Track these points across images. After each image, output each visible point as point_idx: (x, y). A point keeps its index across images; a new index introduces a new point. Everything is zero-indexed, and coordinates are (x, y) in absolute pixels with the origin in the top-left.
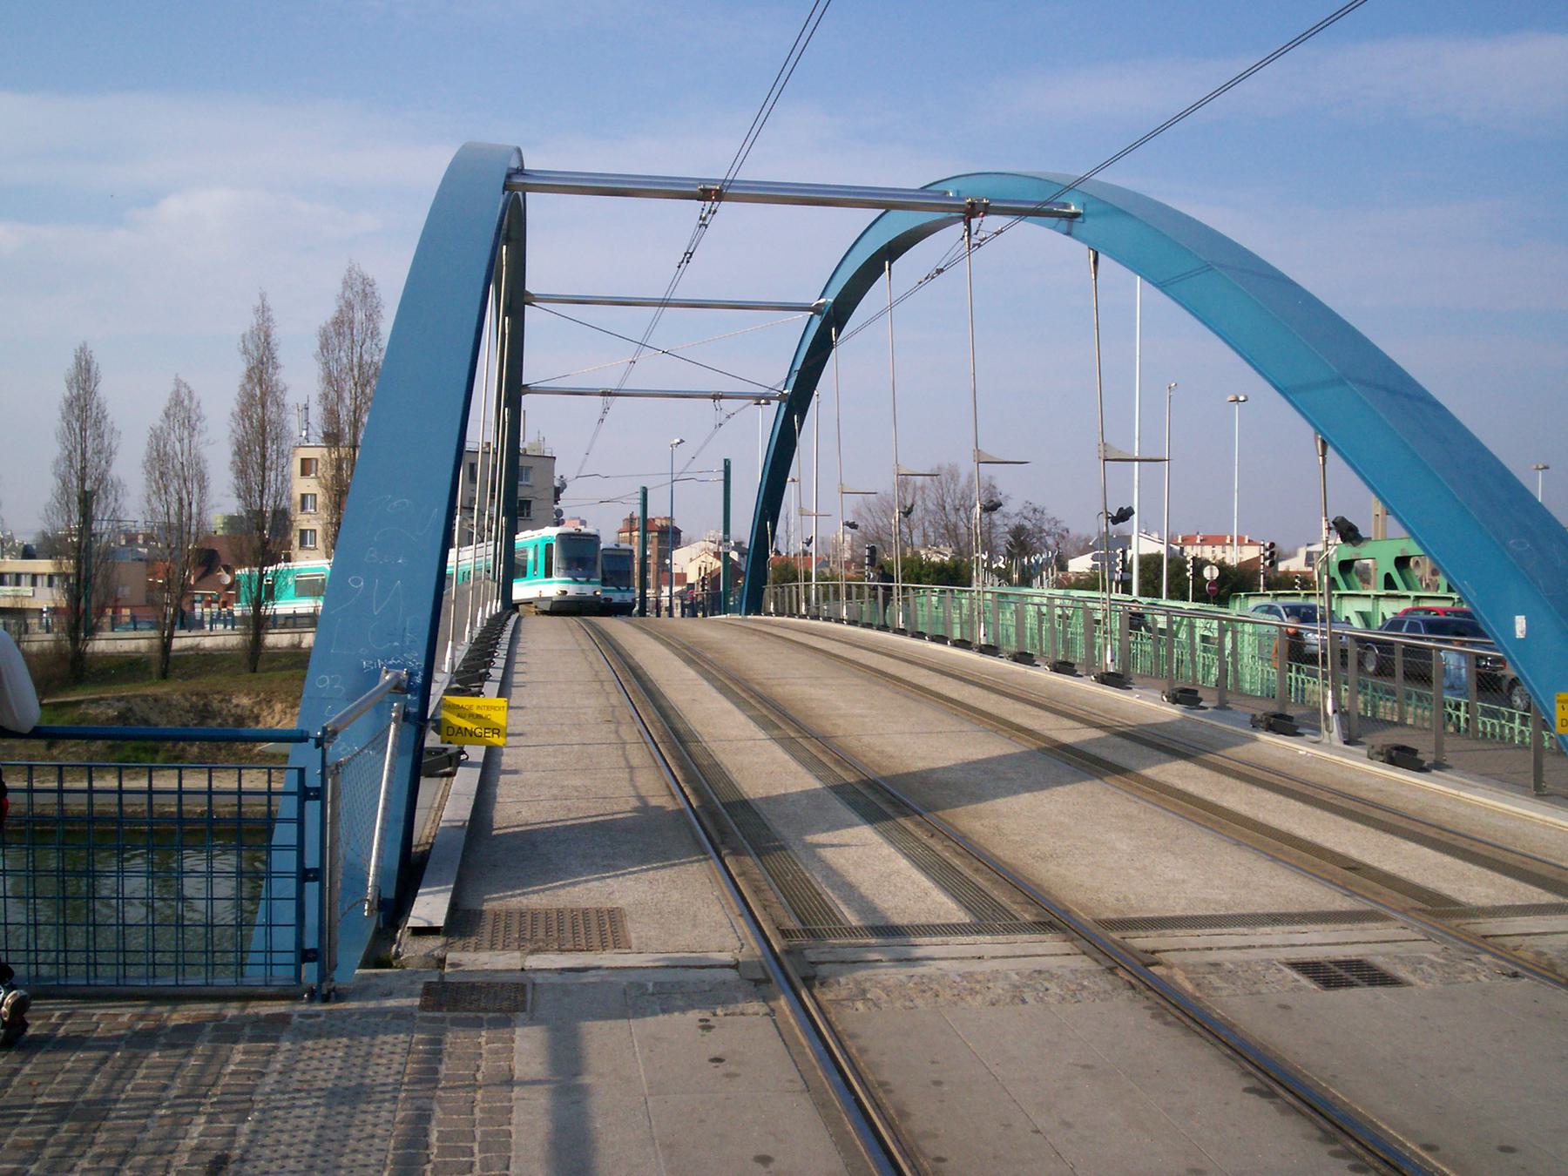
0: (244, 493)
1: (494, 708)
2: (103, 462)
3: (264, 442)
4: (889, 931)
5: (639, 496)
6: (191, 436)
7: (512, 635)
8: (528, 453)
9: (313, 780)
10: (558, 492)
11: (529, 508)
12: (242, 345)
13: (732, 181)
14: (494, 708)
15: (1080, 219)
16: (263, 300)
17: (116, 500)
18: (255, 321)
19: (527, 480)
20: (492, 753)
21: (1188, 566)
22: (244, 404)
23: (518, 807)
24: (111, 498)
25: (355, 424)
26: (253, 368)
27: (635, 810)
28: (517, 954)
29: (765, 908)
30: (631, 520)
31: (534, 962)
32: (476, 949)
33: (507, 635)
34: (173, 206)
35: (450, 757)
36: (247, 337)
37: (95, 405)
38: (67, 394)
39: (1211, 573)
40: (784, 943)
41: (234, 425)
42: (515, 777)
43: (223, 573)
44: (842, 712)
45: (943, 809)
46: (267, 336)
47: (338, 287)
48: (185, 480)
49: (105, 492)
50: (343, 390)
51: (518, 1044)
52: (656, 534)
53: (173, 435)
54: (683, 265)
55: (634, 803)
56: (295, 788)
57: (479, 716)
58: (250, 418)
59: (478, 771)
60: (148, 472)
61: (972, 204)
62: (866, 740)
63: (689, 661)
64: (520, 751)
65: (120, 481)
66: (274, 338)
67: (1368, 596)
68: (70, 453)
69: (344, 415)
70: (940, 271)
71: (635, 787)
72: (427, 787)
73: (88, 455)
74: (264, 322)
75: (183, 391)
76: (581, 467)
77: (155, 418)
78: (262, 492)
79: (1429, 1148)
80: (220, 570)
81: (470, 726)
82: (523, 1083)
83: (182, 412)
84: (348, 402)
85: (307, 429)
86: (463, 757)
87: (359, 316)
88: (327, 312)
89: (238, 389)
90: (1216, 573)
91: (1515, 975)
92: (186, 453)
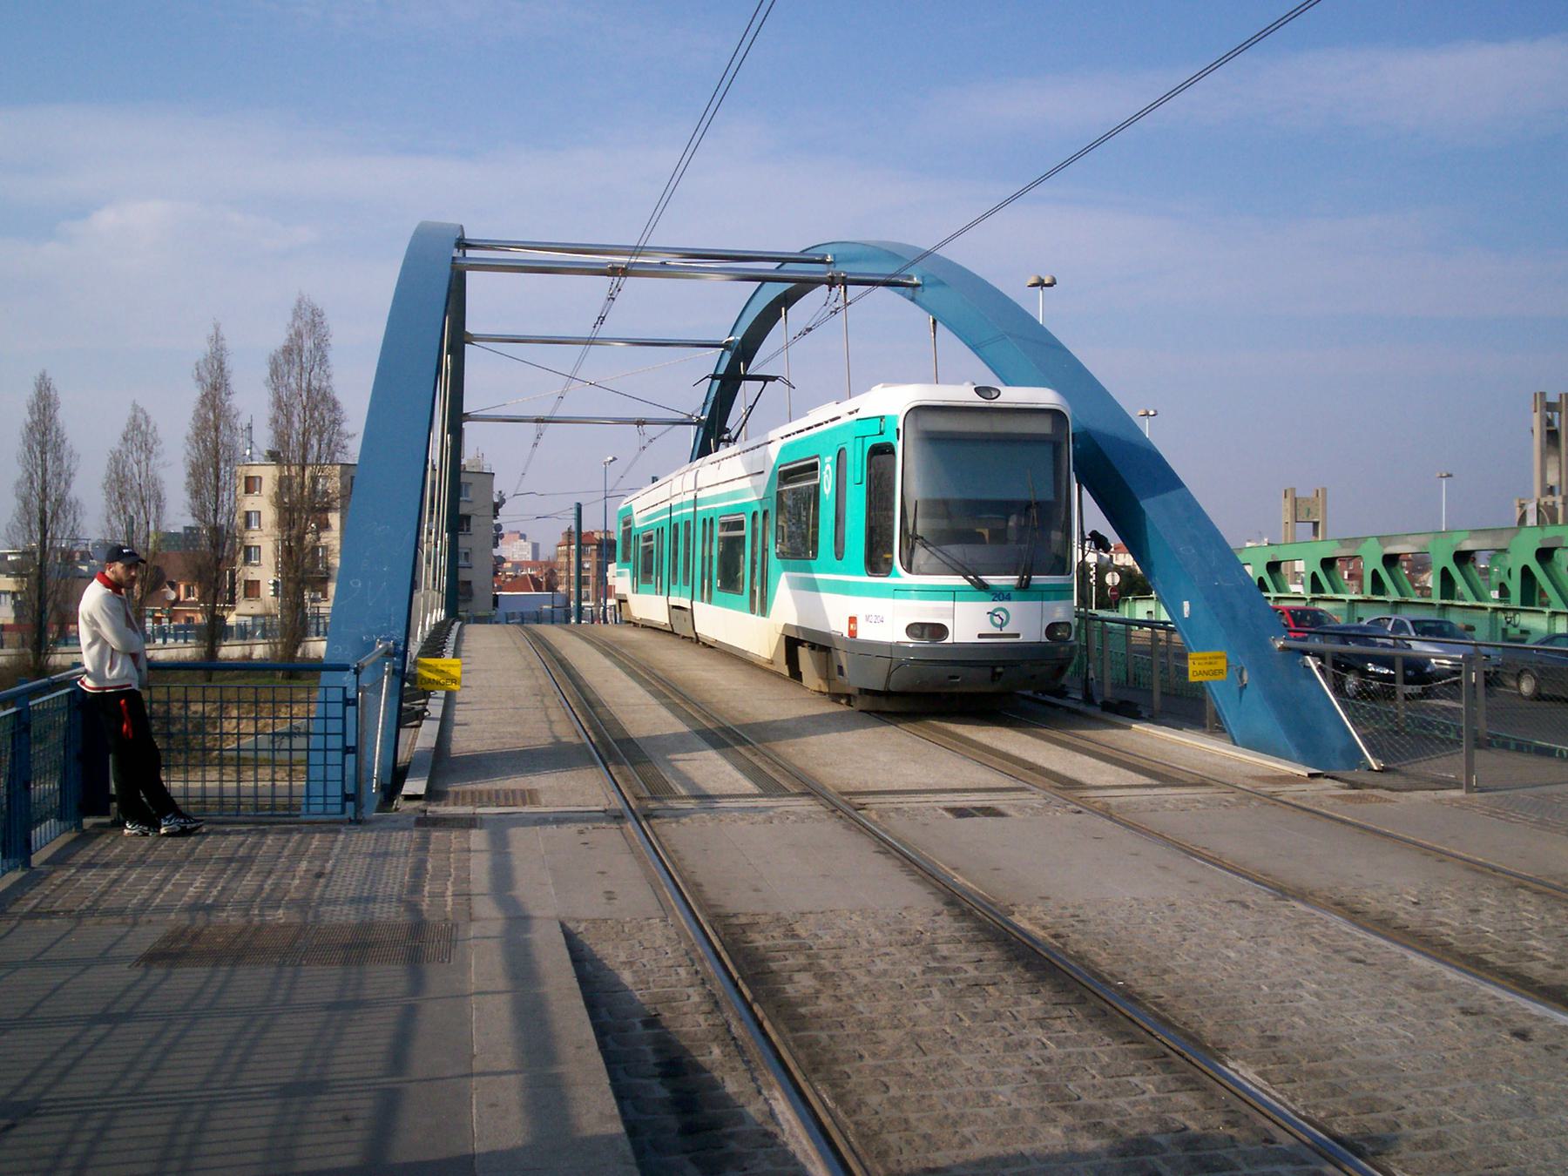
0: (200, 513)
1: (452, 666)
2: (63, 484)
3: (217, 463)
4: (703, 797)
5: (574, 511)
6: (148, 458)
7: (457, 636)
8: (467, 470)
9: (351, 694)
10: (497, 507)
11: (468, 524)
12: (196, 372)
13: (642, 248)
14: (452, 666)
15: (920, 288)
16: (217, 329)
17: (75, 520)
18: (209, 349)
19: (467, 495)
20: (450, 698)
21: (1091, 573)
22: (198, 428)
23: (467, 743)
24: (70, 517)
25: (305, 446)
26: (206, 395)
27: (551, 743)
28: (471, 807)
29: (629, 788)
30: (569, 533)
31: (480, 810)
32: (446, 805)
33: (453, 636)
34: (106, 219)
35: (417, 712)
36: (201, 364)
37: (54, 429)
38: (29, 419)
39: (1113, 579)
40: (637, 802)
41: (189, 447)
42: (465, 727)
43: (168, 589)
44: (721, 687)
45: (770, 741)
46: (221, 363)
47: (290, 319)
48: (143, 502)
49: (64, 512)
50: (292, 415)
51: (472, 838)
52: (595, 547)
53: (131, 458)
54: (598, 326)
55: (551, 740)
56: (341, 699)
57: (443, 671)
58: (204, 441)
59: (438, 723)
60: (108, 493)
61: (832, 277)
62: (732, 704)
63: (607, 654)
64: (468, 713)
65: (77, 501)
66: (228, 365)
67: (1343, 600)
68: (31, 475)
69: (295, 439)
70: (809, 330)
71: (552, 732)
72: (405, 734)
73: (48, 478)
74: (217, 350)
75: (140, 415)
76: (519, 485)
77: (113, 441)
78: (216, 511)
79: (954, 869)
80: (165, 587)
81: (436, 677)
82: (475, 851)
83: (139, 435)
84: (297, 425)
85: (250, 448)
86: (426, 714)
87: (308, 344)
88: (278, 338)
89: (193, 415)
90: (1117, 579)
91: (1079, 812)
92: (144, 474)
